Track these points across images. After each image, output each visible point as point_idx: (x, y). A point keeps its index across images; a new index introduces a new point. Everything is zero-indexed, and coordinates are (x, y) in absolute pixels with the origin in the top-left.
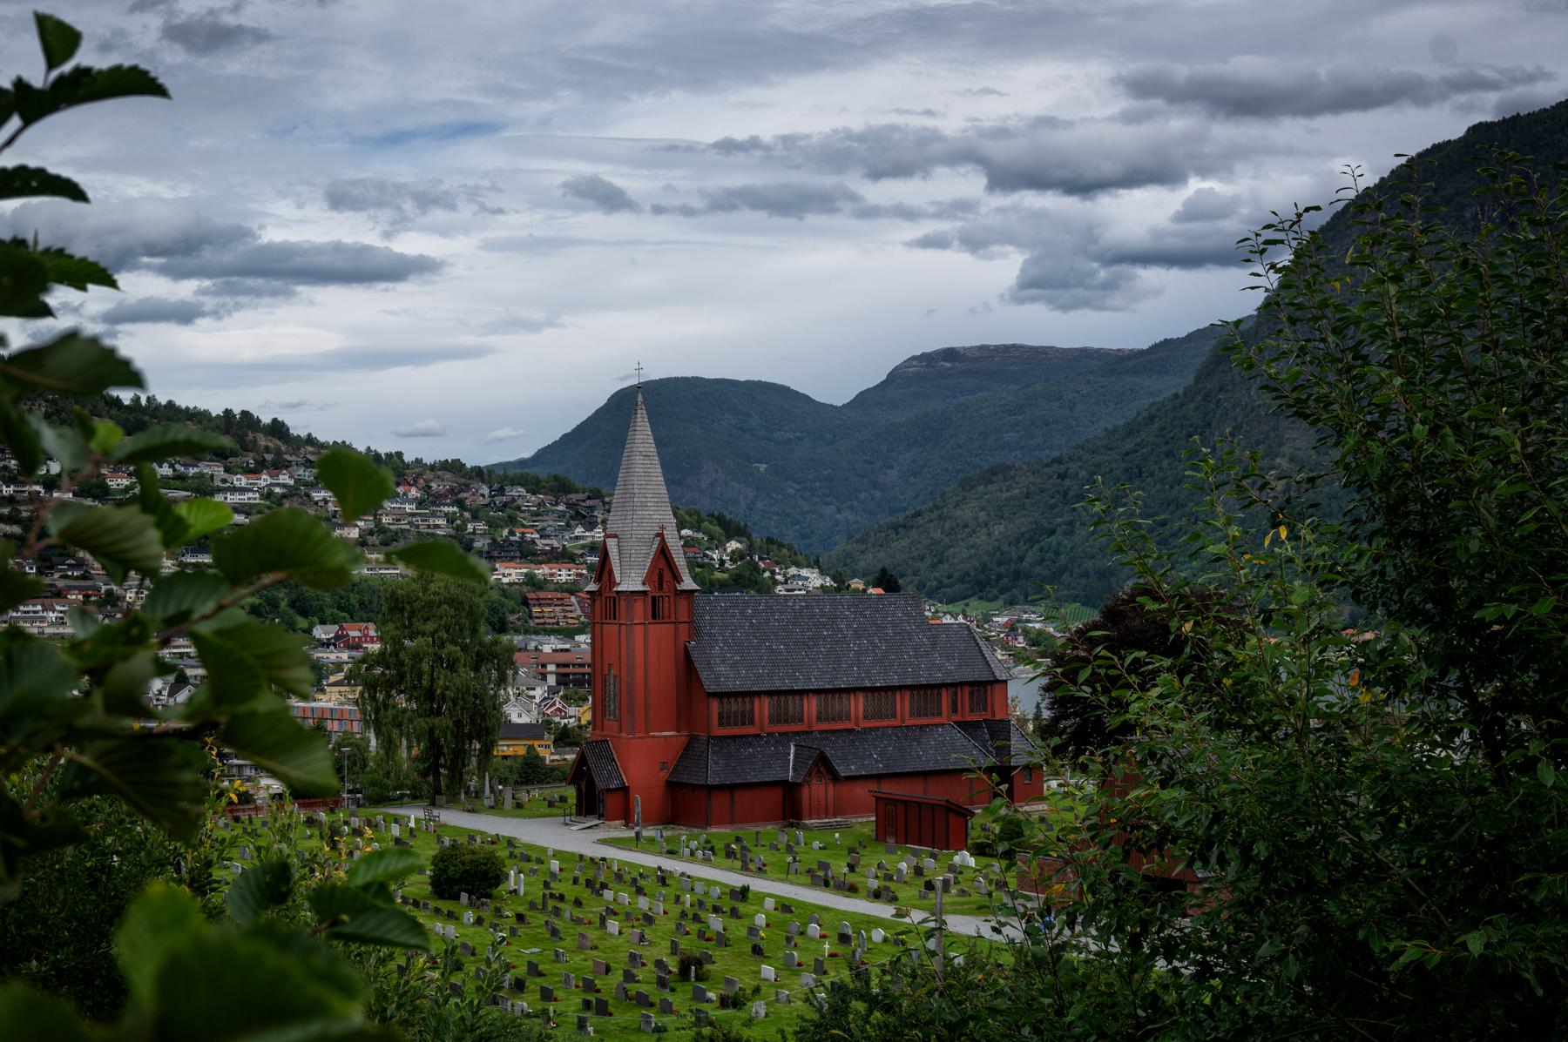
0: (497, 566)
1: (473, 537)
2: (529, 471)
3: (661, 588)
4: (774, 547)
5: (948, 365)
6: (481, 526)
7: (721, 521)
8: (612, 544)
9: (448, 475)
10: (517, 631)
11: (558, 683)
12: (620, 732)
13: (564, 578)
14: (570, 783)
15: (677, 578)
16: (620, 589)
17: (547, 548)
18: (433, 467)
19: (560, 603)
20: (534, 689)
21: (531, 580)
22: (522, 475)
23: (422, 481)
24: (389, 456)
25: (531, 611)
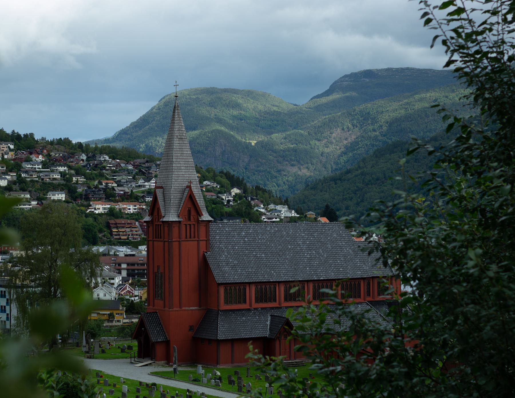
0: (91, 203)
1: (77, 185)
2: (111, 145)
3: (189, 219)
4: (260, 192)
5: (367, 80)
6: (82, 179)
7: (228, 176)
8: (159, 192)
9: (62, 148)
10: (104, 244)
11: (128, 275)
12: (165, 307)
13: (132, 211)
14: (134, 339)
15: (199, 214)
16: (164, 220)
17: (122, 192)
18: (52, 143)
19: (129, 226)
20: (113, 279)
21: (111, 213)
22: (106, 146)
23: (45, 151)
24: (26, 136)
25: (111, 231)
